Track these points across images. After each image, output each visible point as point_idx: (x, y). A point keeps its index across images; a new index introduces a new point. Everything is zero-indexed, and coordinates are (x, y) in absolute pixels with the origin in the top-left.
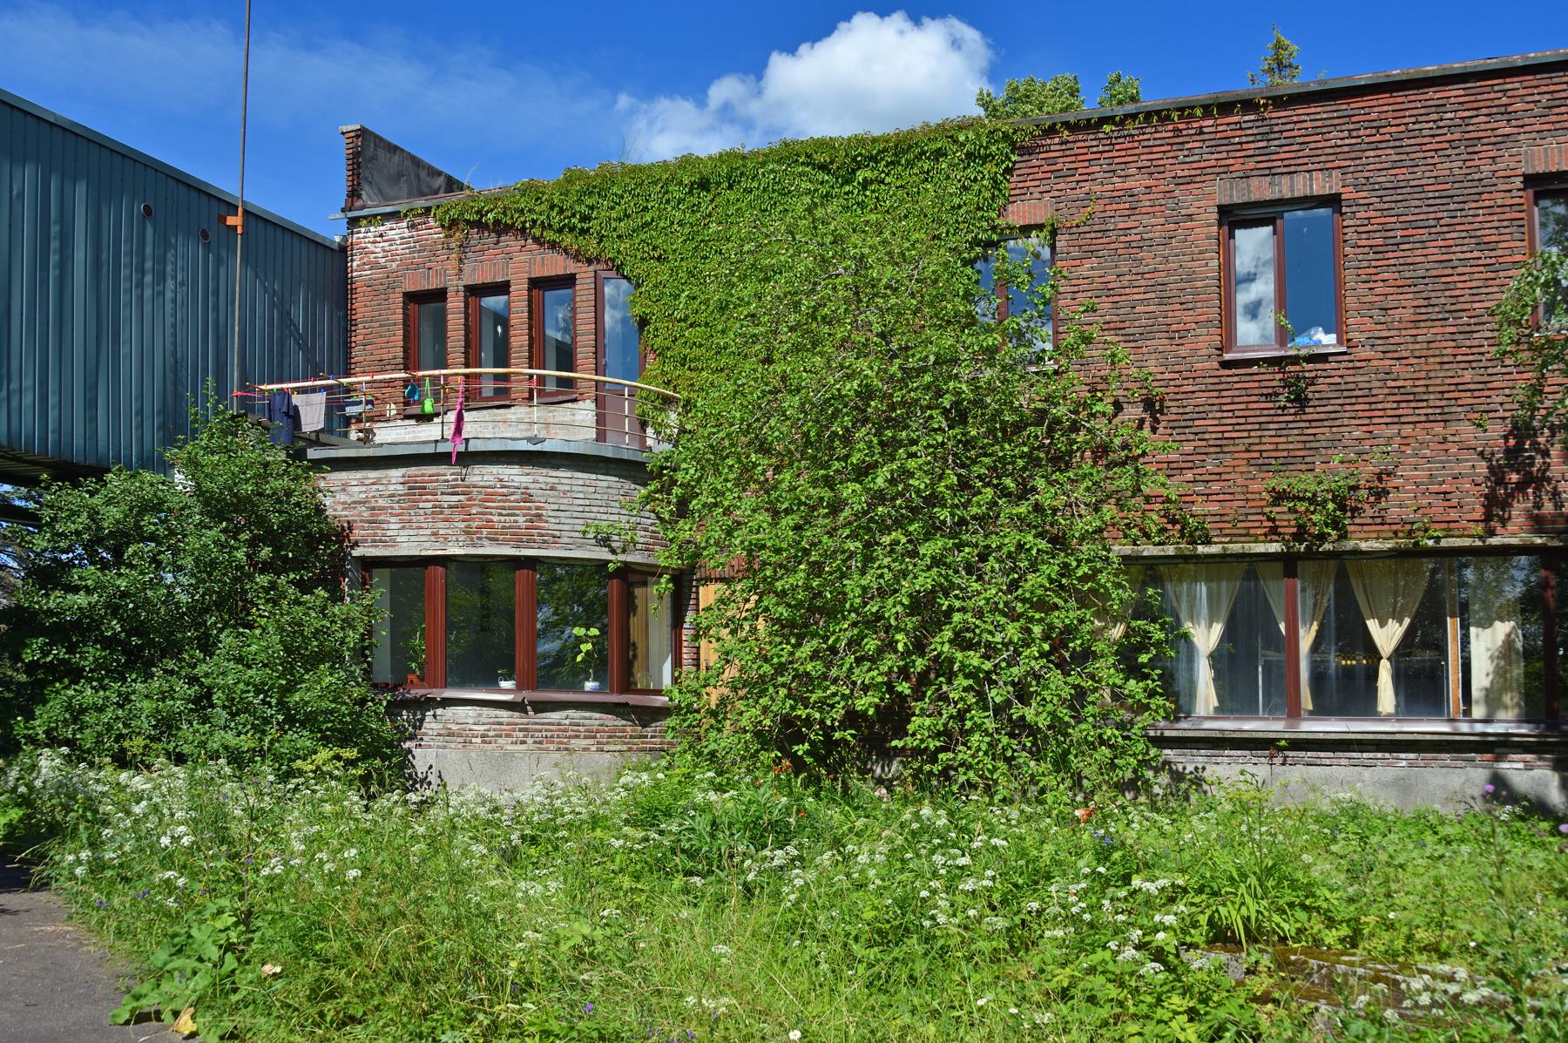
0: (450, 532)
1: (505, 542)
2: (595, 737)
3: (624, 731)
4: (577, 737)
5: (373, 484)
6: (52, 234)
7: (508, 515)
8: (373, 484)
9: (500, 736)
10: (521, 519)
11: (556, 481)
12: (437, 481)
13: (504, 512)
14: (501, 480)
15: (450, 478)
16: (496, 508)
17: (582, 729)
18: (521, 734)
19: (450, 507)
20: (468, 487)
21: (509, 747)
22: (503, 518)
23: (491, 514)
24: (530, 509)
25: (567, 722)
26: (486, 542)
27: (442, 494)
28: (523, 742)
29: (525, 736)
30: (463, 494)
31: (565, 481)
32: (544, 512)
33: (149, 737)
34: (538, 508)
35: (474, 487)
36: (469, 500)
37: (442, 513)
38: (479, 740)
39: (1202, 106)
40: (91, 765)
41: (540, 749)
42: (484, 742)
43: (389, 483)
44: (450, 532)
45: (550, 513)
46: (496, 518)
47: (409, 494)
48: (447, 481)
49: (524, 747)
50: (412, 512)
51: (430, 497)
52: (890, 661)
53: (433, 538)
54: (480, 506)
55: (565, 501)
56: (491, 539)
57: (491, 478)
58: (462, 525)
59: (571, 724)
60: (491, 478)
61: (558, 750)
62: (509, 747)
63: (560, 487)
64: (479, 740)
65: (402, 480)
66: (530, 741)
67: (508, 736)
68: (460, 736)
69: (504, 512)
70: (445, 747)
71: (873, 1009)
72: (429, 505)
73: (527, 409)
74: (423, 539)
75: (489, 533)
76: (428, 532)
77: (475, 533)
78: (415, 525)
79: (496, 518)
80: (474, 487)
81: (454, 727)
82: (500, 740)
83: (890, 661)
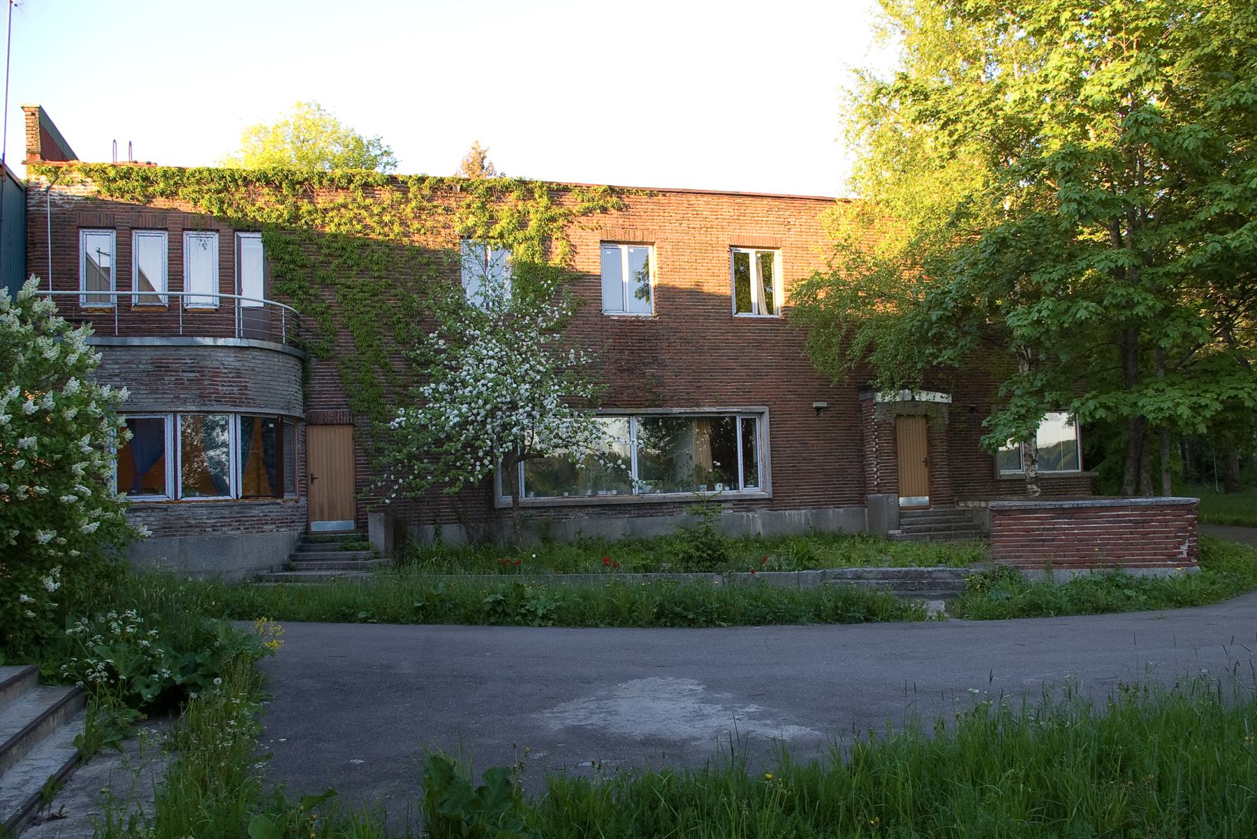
0: (188, 396)
2: (275, 523)
3: (287, 519)
4: (267, 523)
6: (212, 344)
9: (224, 526)
10: (236, 389)
11: (254, 365)
12: (178, 363)
13: (226, 384)
14: (223, 364)
15: (189, 361)
16: (221, 381)
17: (269, 518)
18: (237, 524)
21: (229, 533)
22: (225, 388)
23: (217, 385)
24: (241, 382)
25: (261, 515)
26: (214, 403)
27: (183, 371)
28: (239, 529)
29: (239, 525)
30: (198, 372)
31: (260, 366)
32: (248, 384)
33: (1195, 316)
34: (245, 382)
35: (206, 367)
36: (203, 376)
37: (182, 384)
38: (210, 529)
41: (248, 532)
42: (213, 530)
44: (188, 396)
45: (252, 385)
46: (220, 388)
48: (187, 363)
49: (238, 532)
51: (173, 373)
52: (1023, 198)
54: (210, 380)
55: (259, 378)
56: (217, 401)
58: (198, 392)
59: (264, 516)
60: (217, 363)
61: (258, 532)
62: (229, 533)
63: (256, 369)
64: (210, 529)
66: (242, 528)
67: (228, 525)
68: (196, 527)
69: (226, 384)
70: (186, 535)
71: (422, 209)
72: (173, 378)
77: (207, 397)
78: (160, 392)
79: (220, 388)
80: (206, 367)
81: (193, 522)
82: (223, 528)
83: (1023, 198)
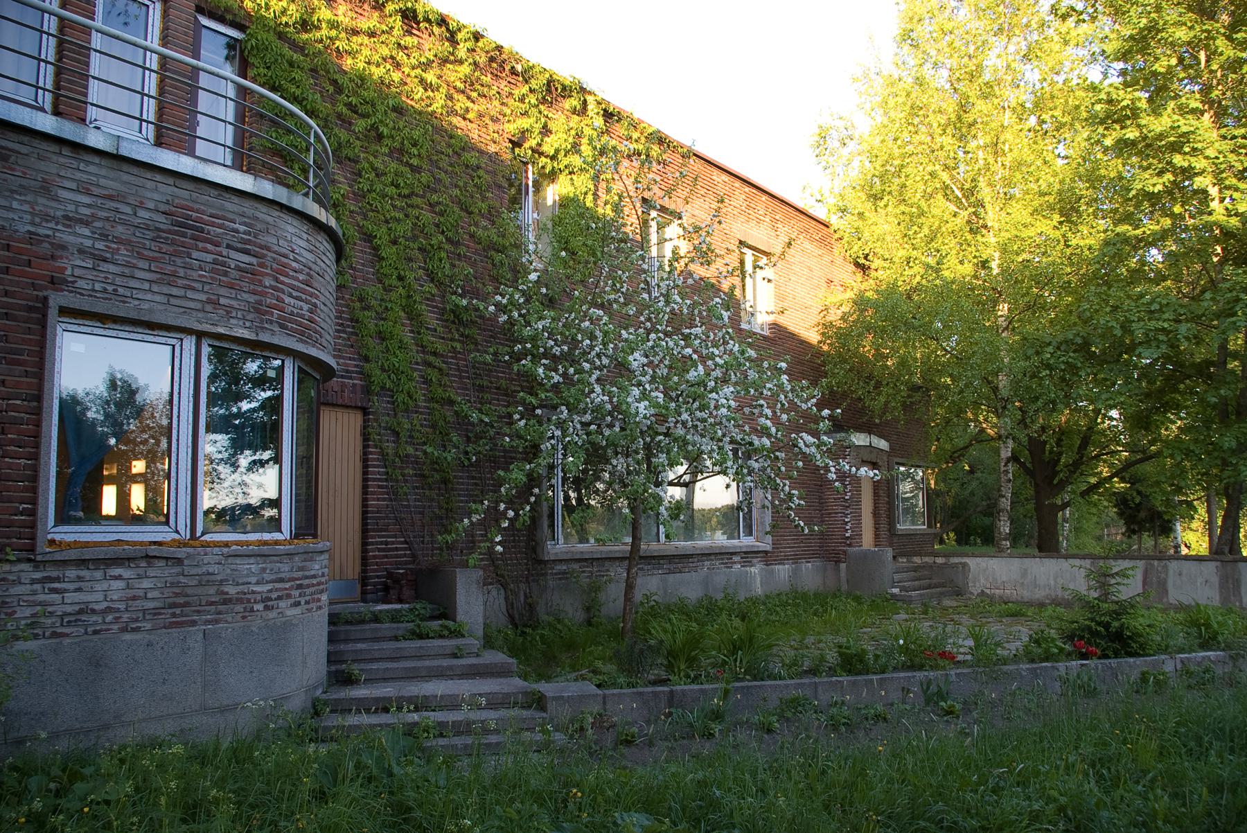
1: (291, 333)
5: (110, 198)
7: (296, 298)
8: (110, 198)
10: (306, 307)
19: (238, 269)
20: (261, 247)
27: (228, 247)
35: (268, 249)
37: (226, 274)
38: (260, 607)
39: (467, 567)
40: (1094, 88)
42: (267, 608)
43: (141, 206)
44: (234, 303)
46: (287, 300)
47: (176, 233)
48: (237, 231)
50: (179, 261)
51: (209, 247)
53: (209, 308)
57: (285, 245)
58: (252, 299)
65: (163, 207)
68: (240, 601)
70: (217, 621)
72: (210, 258)
73: (758, 314)
74: (192, 305)
75: (280, 317)
76: (203, 297)
78: (180, 282)
79: (287, 300)
